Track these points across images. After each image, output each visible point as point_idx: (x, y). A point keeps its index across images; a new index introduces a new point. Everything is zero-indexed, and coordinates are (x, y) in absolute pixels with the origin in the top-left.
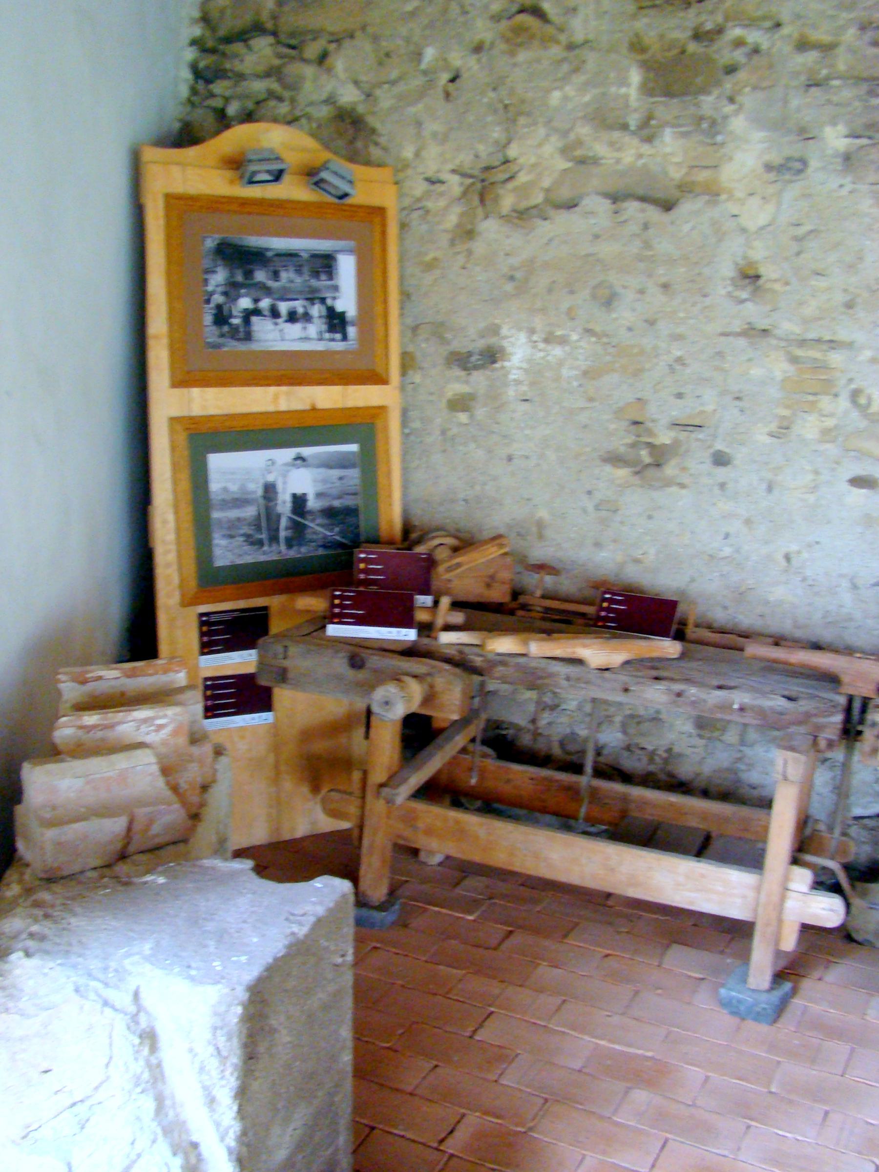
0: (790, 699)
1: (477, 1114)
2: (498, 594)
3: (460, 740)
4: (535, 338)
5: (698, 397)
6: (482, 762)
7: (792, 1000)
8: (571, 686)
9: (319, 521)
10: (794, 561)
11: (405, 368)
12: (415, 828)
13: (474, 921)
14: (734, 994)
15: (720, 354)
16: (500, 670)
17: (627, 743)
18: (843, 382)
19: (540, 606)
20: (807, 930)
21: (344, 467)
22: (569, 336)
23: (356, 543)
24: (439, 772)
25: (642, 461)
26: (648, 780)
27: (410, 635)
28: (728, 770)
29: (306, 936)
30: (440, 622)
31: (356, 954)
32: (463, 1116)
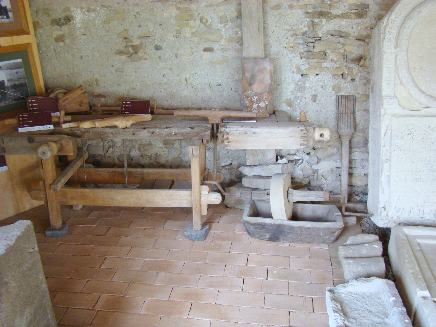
0: (192, 128)
1: (105, 294)
2: (85, 108)
3: (79, 163)
4: (84, 10)
5: (147, 26)
6: (89, 170)
7: (210, 231)
8: (114, 136)
9: (11, 90)
11: (35, 28)
13: (96, 226)
15: (152, 9)
16: (87, 135)
17: (141, 154)
18: (197, 14)
19: (101, 110)
20: (210, 206)
21: (18, 68)
22: (96, 8)
23: (27, 96)
24: (73, 176)
25: (130, 52)
26: (151, 166)
27: (51, 127)
28: (177, 157)
29: (14, 244)
30: (62, 120)
31: (39, 246)
32: (100, 296)
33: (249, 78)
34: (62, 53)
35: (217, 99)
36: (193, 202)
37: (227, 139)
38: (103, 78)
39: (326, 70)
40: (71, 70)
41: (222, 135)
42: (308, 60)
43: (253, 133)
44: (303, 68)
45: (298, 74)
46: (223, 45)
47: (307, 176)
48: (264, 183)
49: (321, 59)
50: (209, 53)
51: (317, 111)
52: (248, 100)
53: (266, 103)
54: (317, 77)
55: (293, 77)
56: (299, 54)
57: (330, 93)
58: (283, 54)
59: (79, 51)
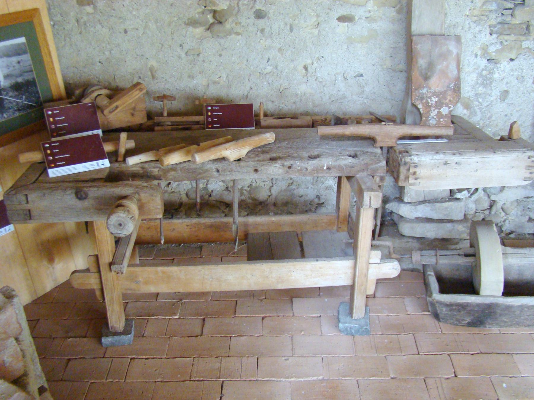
9: (11, 94)
10: (309, 69)
12: (137, 282)
13: (179, 318)
14: (347, 325)
17: (225, 187)
21: (19, 54)
27: (105, 163)
33: (423, 67)
34: (90, 25)
35: (355, 97)
36: (357, 278)
37: (415, 173)
38: (164, 65)
39: (525, 52)
40: (107, 53)
41: (406, 168)
42: (501, 37)
43: (456, 163)
44: (492, 49)
45: (484, 59)
46: (370, 12)
47: (481, 210)
48: (434, 229)
49: (521, 35)
50: (346, 24)
51: (506, 115)
52: (422, 103)
53: (450, 107)
54: (512, 63)
55: (476, 63)
56: (488, 27)
57: (529, 87)
58: (463, 27)
59: (120, 21)
